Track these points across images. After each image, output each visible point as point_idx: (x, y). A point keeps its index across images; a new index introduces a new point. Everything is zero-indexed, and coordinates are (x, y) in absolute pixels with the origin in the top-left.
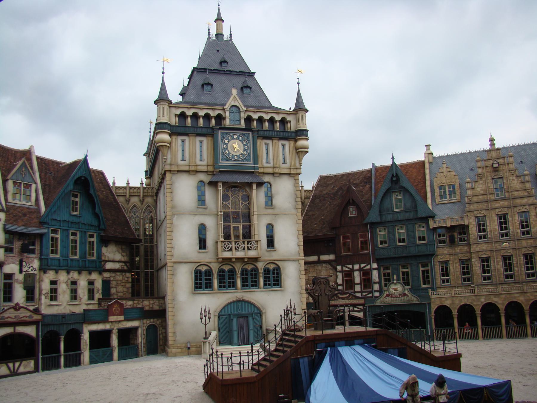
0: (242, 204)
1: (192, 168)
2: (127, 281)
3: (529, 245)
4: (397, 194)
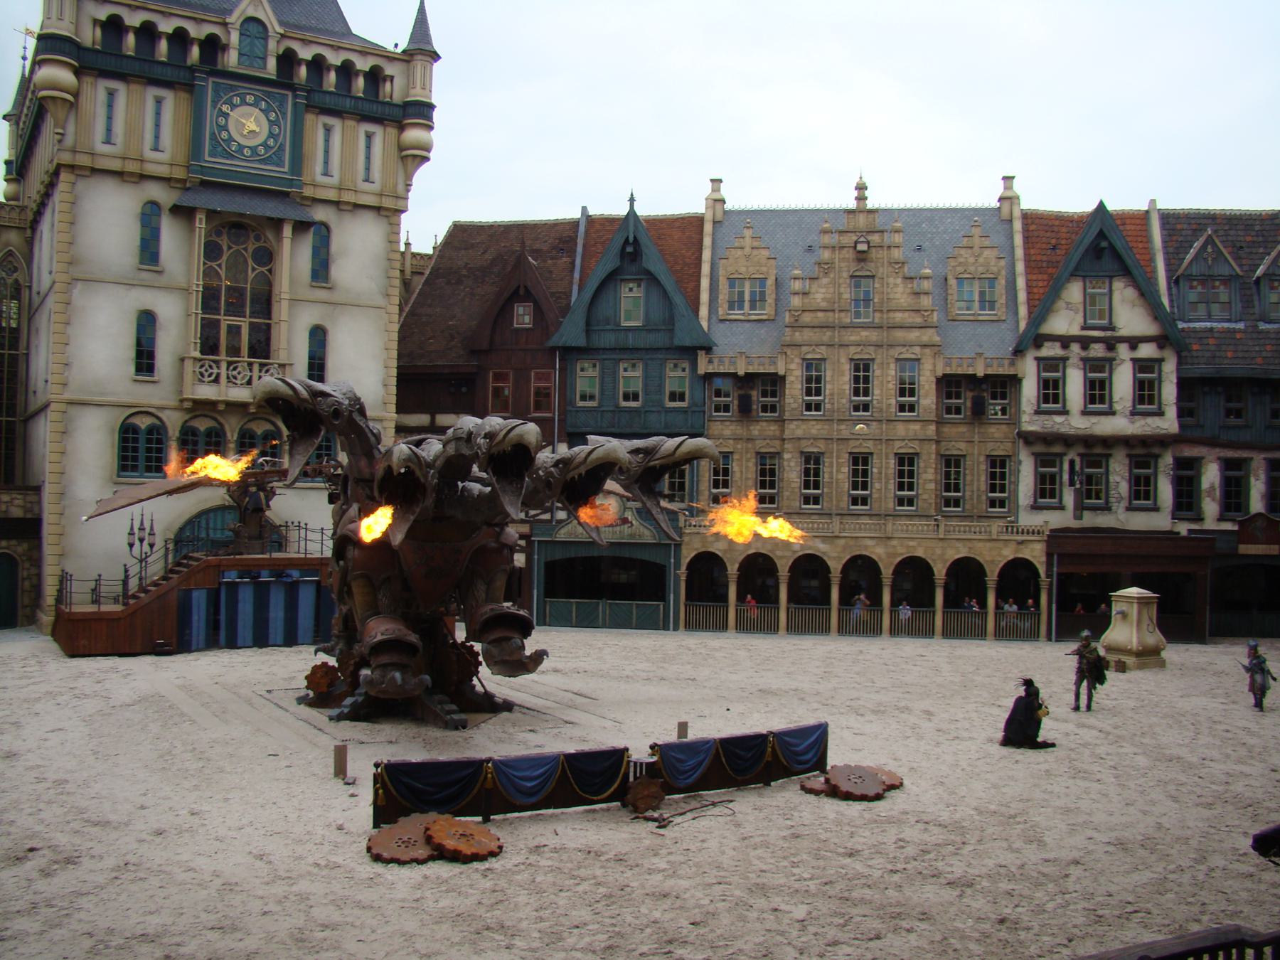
0: (254, 269)
1: (132, 167)
3: (911, 435)
4: (631, 285)
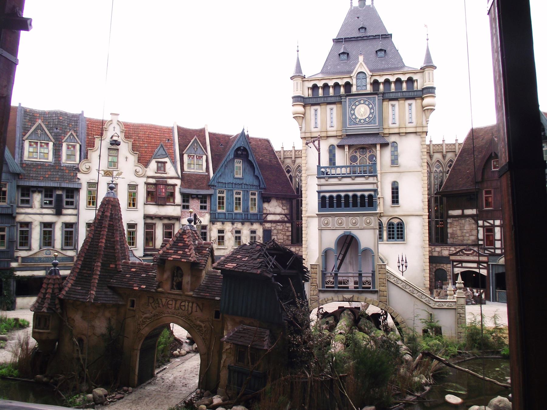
2: (288, 231)
